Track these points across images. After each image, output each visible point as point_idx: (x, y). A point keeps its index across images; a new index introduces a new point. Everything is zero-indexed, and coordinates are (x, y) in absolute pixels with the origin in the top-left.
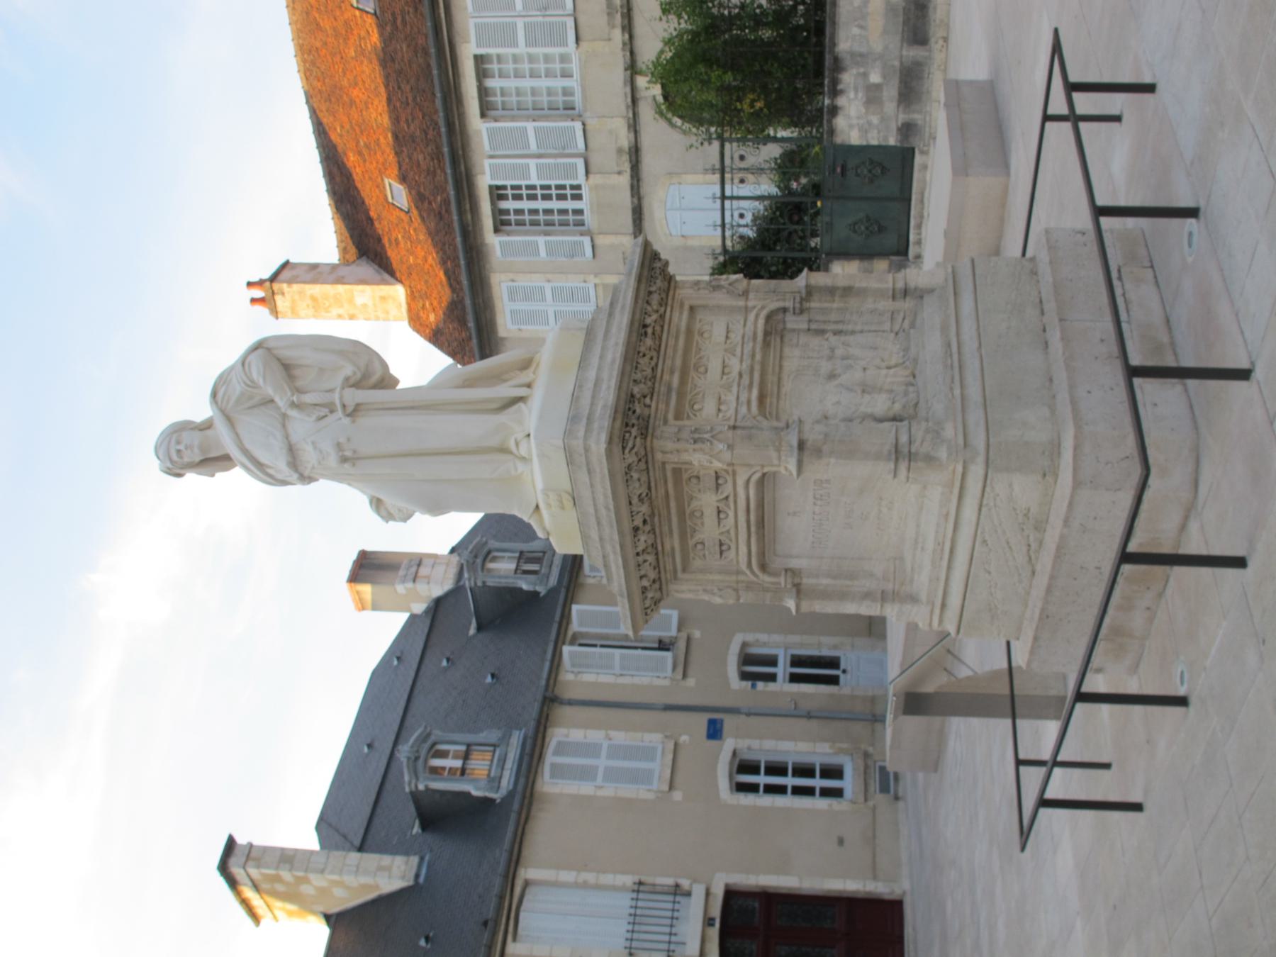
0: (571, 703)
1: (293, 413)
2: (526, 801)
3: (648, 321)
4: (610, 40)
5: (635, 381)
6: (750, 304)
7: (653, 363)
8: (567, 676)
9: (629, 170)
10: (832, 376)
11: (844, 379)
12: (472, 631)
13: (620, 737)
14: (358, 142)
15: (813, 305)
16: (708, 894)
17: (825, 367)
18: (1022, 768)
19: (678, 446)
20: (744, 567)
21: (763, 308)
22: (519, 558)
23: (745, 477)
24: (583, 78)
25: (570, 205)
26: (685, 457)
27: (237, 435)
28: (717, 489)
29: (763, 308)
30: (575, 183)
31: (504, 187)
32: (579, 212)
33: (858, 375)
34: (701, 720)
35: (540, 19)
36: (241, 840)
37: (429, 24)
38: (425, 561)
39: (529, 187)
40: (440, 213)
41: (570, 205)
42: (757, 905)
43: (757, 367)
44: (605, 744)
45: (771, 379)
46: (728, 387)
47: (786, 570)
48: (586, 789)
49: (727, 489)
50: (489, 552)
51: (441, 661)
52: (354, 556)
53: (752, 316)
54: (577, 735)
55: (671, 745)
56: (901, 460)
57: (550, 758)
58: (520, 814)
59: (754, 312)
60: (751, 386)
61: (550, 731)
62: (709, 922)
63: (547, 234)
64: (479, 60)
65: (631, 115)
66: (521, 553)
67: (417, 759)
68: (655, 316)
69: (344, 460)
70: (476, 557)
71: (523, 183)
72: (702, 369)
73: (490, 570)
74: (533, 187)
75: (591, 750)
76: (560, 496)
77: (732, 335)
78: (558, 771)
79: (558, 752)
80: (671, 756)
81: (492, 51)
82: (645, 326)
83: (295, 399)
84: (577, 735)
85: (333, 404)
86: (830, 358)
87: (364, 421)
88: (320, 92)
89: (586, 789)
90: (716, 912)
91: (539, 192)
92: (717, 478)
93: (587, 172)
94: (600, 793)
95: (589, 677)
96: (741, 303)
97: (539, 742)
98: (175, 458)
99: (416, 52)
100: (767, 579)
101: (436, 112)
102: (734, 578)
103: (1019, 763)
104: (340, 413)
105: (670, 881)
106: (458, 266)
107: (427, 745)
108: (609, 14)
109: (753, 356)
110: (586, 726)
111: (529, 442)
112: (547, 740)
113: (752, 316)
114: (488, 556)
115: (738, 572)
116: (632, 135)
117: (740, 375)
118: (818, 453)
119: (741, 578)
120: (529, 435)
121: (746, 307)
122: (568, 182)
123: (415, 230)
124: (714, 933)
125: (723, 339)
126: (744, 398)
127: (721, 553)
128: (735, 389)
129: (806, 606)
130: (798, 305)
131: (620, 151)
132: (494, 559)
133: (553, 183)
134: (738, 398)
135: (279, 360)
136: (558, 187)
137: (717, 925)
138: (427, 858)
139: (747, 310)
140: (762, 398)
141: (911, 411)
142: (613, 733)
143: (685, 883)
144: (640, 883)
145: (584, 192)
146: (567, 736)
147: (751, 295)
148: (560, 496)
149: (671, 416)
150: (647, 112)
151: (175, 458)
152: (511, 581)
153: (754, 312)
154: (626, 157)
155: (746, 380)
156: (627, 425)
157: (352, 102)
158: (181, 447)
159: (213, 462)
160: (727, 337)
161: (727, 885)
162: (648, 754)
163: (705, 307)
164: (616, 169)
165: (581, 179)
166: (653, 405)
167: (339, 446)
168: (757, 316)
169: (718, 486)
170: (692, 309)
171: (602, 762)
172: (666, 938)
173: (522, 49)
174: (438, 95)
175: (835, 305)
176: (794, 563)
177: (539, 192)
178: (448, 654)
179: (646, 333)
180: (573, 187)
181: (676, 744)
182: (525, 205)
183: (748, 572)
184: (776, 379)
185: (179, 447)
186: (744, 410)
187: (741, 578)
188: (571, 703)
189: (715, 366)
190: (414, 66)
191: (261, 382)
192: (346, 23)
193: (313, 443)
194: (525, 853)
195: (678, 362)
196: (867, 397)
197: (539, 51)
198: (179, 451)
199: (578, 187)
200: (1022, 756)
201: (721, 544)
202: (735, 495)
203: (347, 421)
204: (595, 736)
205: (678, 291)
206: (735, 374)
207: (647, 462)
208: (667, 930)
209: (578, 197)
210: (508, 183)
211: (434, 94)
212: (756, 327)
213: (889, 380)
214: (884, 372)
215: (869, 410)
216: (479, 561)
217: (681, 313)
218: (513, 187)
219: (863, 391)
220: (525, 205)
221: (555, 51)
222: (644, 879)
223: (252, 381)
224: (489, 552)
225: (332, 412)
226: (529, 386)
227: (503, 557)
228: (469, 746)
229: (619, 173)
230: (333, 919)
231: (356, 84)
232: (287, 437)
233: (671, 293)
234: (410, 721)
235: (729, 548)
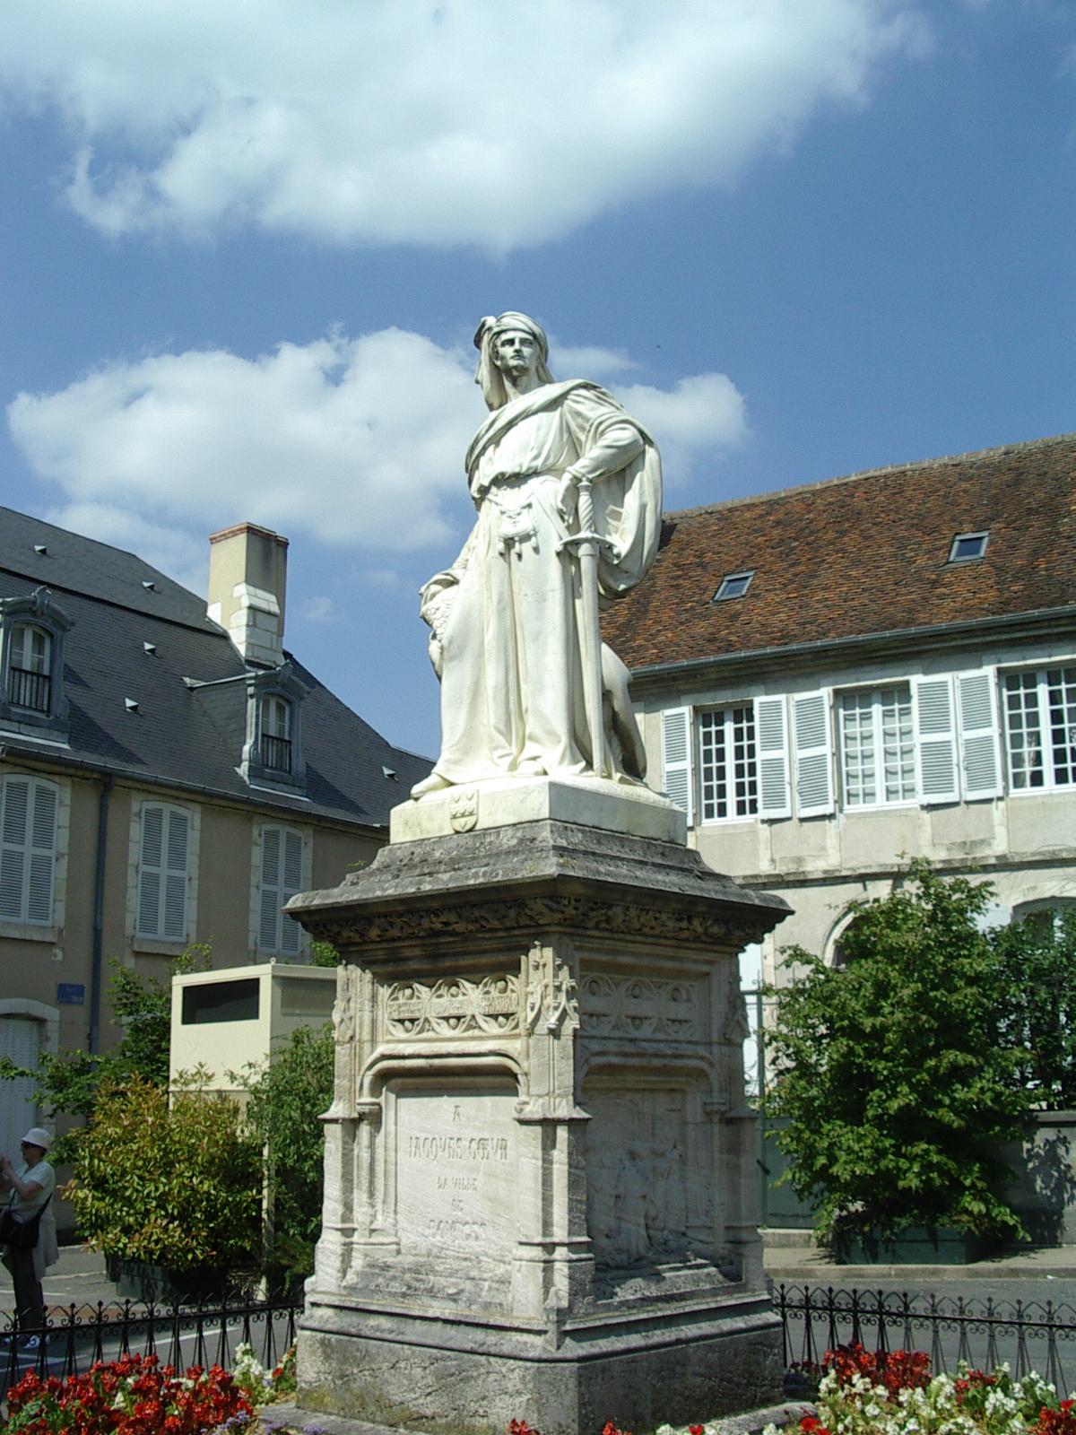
0: (103, 809)
1: (566, 479)
3: (696, 922)
4: (934, 845)
5: (628, 909)
6: (715, 1049)
7: (647, 930)
8: (139, 805)
9: (777, 872)
13: (60, 871)
14: (796, 539)
15: (716, 1128)
17: (641, 1147)
20: (382, 1049)
21: (711, 1064)
23: (511, 1052)
24: (886, 813)
25: (731, 799)
27: (536, 412)
28: (443, 1018)
29: (711, 1064)
30: (760, 805)
31: (751, 718)
32: (722, 811)
34: (82, 977)
35: (955, 762)
37: (944, 626)
39: (752, 749)
40: (715, 639)
41: (731, 799)
43: (644, 1062)
44: (51, 853)
45: (631, 1080)
48: (256, 877)
49: (492, 1028)
50: (290, 703)
51: (150, 643)
54: (62, 816)
55: (48, 938)
57: (284, 830)
60: (626, 1055)
61: (68, 781)
63: (696, 770)
64: (903, 691)
65: (844, 873)
66: (290, 742)
67: (34, 613)
68: (700, 930)
69: (509, 542)
70: (284, 686)
71: (757, 742)
74: (752, 753)
75: (44, 836)
76: (471, 814)
78: (272, 837)
79: (42, 793)
80: (36, 937)
81: (915, 704)
82: (690, 919)
83: (585, 483)
84: (62, 816)
85: (579, 530)
87: (554, 568)
88: (852, 496)
89: (256, 877)
91: (746, 761)
92: (507, 1016)
93: (772, 822)
94: (131, 871)
95: (137, 831)
96: (715, 1038)
97: (56, 768)
98: (504, 337)
99: (910, 611)
101: (840, 635)
104: (568, 538)
106: (652, 663)
107: (49, 626)
108: (965, 843)
109: (656, 1056)
110: (74, 828)
111: (537, 774)
112: (56, 778)
113: (701, 1051)
116: (820, 875)
117: (632, 1040)
119: (367, 1046)
120: (545, 773)
121: (710, 1044)
122: (759, 796)
123: (692, 608)
125: (672, 1017)
126: (611, 1046)
127: (401, 1021)
128: (617, 1034)
129: (333, 1135)
130: (716, 1108)
131: (800, 860)
132: (280, 708)
133: (759, 778)
134: (605, 1038)
135: (630, 465)
136: (753, 785)
140: (611, 1069)
142: (65, 862)
145: (748, 818)
146: (61, 803)
147: (725, 1049)
148: (471, 814)
149: (586, 955)
150: (852, 891)
151: (504, 337)
154: (792, 868)
155: (629, 1048)
156: (577, 901)
157: (843, 533)
158: (517, 346)
160: (674, 1021)
162: (39, 909)
164: (777, 857)
165: (763, 813)
167: (526, 538)
168: (702, 1058)
169: (495, 1017)
171: (164, 872)
173: (919, 738)
174: (861, 637)
175: (717, 1155)
177: (746, 761)
178: (158, 653)
179: (681, 919)
180: (753, 803)
181: (52, 944)
182: (730, 745)
183: (376, 1054)
184: (629, 1085)
185: (517, 341)
187: (367, 1046)
188: (103, 809)
190: (892, 609)
191: (602, 442)
192: (936, 529)
193: (529, 506)
197: (917, 760)
198: (511, 342)
199: (754, 810)
201: (412, 1021)
202: (481, 1038)
203: (558, 546)
204: (61, 839)
206: (635, 1034)
207: (527, 926)
209: (741, 809)
210: (757, 723)
211: (861, 632)
212: (690, 1057)
216: (279, 689)
218: (751, 730)
220: (730, 745)
221: (918, 779)
223: (603, 433)
225: (568, 528)
228: (49, 678)
229: (773, 861)
231: (866, 538)
232: (537, 473)
234: (72, 599)
235: (407, 1031)
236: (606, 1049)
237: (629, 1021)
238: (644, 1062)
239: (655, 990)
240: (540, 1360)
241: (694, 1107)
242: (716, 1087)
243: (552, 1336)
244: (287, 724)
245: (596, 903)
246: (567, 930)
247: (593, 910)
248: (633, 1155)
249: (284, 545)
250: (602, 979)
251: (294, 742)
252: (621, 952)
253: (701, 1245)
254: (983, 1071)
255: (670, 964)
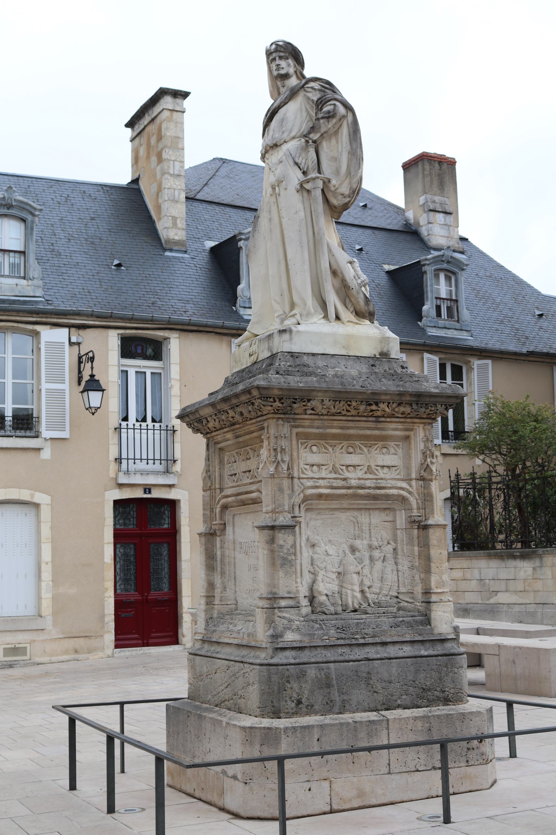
2: (234, 332)
3: (381, 405)
6: (414, 483)
10: (353, 550)
11: (350, 557)
12: (387, 267)
15: (416, 532)
16: (171, 486)
18: (118, 707)
19: (272, 437)
21: (410, 493)
22: (451, 300)
26: (266, 443)
29: (410, 493)
33: (352, 568)
36: (187, 103)
38: (450, 219)
42: (166, 526)
46: (334, 470)
47: (225, 524)
50: (454, 273)
52: (449, 155)
53: (404, 485)
56: (269, 602)
58: (223, 327)
59: (408, 487)
62: (147, 489)
66: (456, 301)
70: (448, 262)
72: (351, 450)
73: (437, 276)
77: (386, 470)
86: (370, 547)
90: (156, 494)
100: (218, 510)
102: (217, 486)
103: (122, 704)
105: (178, 455)
113: (404, 485)
114: (450, 274)
115: (222, 490)
117: (345, 479)
118: (272, 541)
119: (218, 491)
121: (411, 480)
124: (139, 494)
125: (381, 463)
126: (321, 483)
132: (448, 278)
137: (145, 496)
138: (186, 256)
139: (408, 480)
141: (319, 609)
143: (177, 467)
144: (174, 431)
152: (429, 295)
153: (408, 487)
159: (278, 78)
160: (383, 467)
161: (179, 500)
163: (410, 448)
166: (306, 417)
170: (407, 438)
172: (131, 456)
176: (229, 529)
178: (365, 249)
179: (370, 405)
186: (309, 483)
189: (354, 459)
194: (191, 336)
195: (352, 432)
196: (334, 576)
200: (126, 706)
205: (421, 426)
206: (347, 475)
208: (138, 456)
212: (390, 488)
213: (349, 592)
214: (357, 588)
215: (320, 578)
216: (445, 266)
217: (400, 430)
219: (339, 573)
222: (178, 434)
224: (454, 273)
226: (338, 318)
227: (451, 286)
230: (135, 187)
233: (417, 420)
236: (318, 484)
237: (344, 468)
238: (350, 491)
239: (365, 450)
240: (261, 665)
241: (401, 519)
242: (415, 506)
243: (270, 651)
244: (453, 288)
245: (296, 399)
246: (282, 416)
247: (295, 403)
248: (353, 550)
249: (451, 163)
250: (319, 443)
251: (460, 299)
252: (348, 428)
253: (406, 604)
254: (513, 486)
255: (377, 432)
